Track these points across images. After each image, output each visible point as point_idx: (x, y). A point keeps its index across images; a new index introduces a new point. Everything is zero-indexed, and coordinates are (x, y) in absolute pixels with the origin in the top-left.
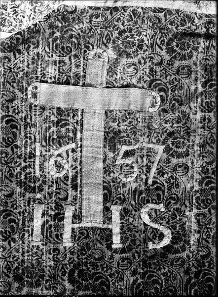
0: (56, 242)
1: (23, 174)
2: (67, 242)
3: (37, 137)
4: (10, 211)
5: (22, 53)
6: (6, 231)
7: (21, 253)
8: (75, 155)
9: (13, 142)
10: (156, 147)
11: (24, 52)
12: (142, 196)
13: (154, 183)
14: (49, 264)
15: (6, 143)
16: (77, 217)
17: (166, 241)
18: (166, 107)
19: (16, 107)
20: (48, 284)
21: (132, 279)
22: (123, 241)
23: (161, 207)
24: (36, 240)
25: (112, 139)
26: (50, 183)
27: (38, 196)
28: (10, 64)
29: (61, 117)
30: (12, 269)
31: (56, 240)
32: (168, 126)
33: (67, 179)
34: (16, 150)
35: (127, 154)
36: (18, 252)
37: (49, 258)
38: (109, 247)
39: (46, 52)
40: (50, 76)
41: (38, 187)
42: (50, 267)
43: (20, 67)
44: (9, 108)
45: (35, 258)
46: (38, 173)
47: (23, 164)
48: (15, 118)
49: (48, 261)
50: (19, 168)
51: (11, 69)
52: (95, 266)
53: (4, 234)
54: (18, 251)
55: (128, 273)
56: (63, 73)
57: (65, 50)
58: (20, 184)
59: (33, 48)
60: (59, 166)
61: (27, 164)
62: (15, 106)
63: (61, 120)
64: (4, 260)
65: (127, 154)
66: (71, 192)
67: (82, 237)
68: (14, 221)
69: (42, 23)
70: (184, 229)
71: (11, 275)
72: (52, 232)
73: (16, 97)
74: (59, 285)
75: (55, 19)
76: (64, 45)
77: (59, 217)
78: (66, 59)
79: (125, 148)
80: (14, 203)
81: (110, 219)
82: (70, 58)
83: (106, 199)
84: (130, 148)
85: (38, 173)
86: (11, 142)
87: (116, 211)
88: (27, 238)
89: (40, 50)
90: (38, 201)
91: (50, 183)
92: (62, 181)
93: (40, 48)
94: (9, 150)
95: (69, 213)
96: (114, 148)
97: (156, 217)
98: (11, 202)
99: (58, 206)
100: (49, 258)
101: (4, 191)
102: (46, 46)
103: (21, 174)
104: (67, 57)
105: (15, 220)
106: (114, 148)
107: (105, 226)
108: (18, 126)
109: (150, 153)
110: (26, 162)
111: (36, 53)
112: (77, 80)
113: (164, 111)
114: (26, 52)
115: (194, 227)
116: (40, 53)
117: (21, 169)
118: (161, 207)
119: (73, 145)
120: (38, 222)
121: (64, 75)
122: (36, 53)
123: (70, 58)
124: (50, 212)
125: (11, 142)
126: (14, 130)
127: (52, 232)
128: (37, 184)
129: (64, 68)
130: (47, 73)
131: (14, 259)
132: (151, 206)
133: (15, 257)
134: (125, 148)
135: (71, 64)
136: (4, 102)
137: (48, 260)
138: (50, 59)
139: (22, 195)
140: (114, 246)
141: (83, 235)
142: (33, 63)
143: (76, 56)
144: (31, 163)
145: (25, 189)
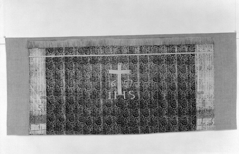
2: (115, 98)
10: (131, 80)
12: (129, 90)
13: (131, 87)
16: (117, 94)
17: (134, 97)
18: (133, 73)
21: (128, 105)
22: (126, 97)
23: (133, 91)
24: (110, 98)
25: (123, 79)
27: (110, 90)
32: (172, 120)
35: (126, 82)
38: (123, 99)
46: (109, 86)
49: (112, 102)
52: (121, 103)
55: (127, 104)
58: (144, 98)
60: (113, 84)
65: (126, 82)
66: (116, 89)
68: (68, 110)
70: (137, 95)
72: (113, 97)
77: (114, 94)
78: (151, 92)
79: (125, 81)
81: (123, 94)
83: (122, 90)
84: (126, 81)
85: (109, 86)
87: (124, 92)
89: (109, 64)
95: (115, 92)
96: (123, 81)
97: (132, 93)
99: (113, 92)
106: (123, 81)
107: (122, 95)
109: (130, 81)
112: (117, 69)
113: (132, 74)
115: (139, 95)
118: (133, 91)
119: (115, 80)
120: (110, 95)
127: (113, 97)
132: (131, 91)
134: (125, 81)
140: (124, 98)
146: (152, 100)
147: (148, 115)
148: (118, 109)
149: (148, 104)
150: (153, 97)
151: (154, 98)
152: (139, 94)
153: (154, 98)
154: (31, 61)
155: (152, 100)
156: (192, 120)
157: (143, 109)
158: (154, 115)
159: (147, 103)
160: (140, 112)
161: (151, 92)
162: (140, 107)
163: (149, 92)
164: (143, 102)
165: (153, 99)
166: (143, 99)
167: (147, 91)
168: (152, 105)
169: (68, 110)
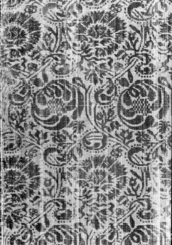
0: (59, 229)
1: (114, 185)
3: (93, 100)
4: (132, 128)
5: (121, 226)
6: (136, 97)
7: (114, 62)
8: (35, 220)
9: (132, 235)
11: (119, 227)
14: (70, 51)
15: (142, 234)
19: (127, 141)
20: (73, 164)
26: (72, 173)
28: (139, 209)
29: (58, 132)
30: (127, 185)
31: (60, 232)
33: (48, 182)
34: (126, 222)
36: (120, 210)
37: (71, 205)
39: (84, 86)
40: (78, 194)
41: (91, 166)
42: (69, 191)
43: (123, 58)
44: (137, 138)
45: (94, 201)
47: (114, 201)
48: (128, 126)
50: (121, 48)
51: (138, 200)
53: (139, 91)
54: (120, 212)
56: (57, 200)
57: (54, 91)
58: (120, 170)
59: (103, 90)
61: (108, 202)
62: (129, 142)
63: (58, 127)
64: (141, 197)
67: (20, 238)
68: (127, 113)
69: (94, 130)
71: (129, 175)
73: (127, 156)
74: (55, 19)
75: (75, 136)
76: (56, 97)
78: (53, 221)
80: (127, 141)
82: (47, 222)
86: (135, 235)
88: (104, 88)
89: (94, 87)
90: (91, 145)
91: (72, 173)
92: (54, 178)
93: (93, 91)
94: (138, 223)
98: (131, 141)
100: (71, 205)
101: (142, 158)
102: (85, 240)
103: (118, 186)
104: (50, 80)
105: (124, 114)
108: (122, 114)
110: (111, 204)
111: (99, 82)
114: (115, 227)
116: (93, 84)
117: (117, 47)
121: (56, 198)
122: (101, 227)
123: (47, 222)
124: (70, 130)
125: (135, 235)
126: (126, 107)
128: (93, 170)
129: (56, 207)
130: (81, 198)
131: (124, 54)
133: (125, 203)
135: (45, 215)
136: (145, 147)
137: (72, 202)
138: (78, 221)
139: (117, 152)
141: (19, 240)
142: (104, 212)
143: (37, 82)
144: (103, 202)
145: (110, 161)
146: (48, 151)
147: (81, 30)
148: (112, 142)
149: (82, 117)
150: (43, 176)
151: (37, 169)
152: (157, 208)
153: (34, 170)
154: (167, 69)
155: (48, 151)
156: (36, 55)
157: (123, 82)
158: (34, 25)
159: (90, 126)
160: (154, 52)
161: (53, 221)
162: (151, 97)
163: (70, 223)
164: (126, 137)
165: (39, 161)
166: (122, 160)
167: (90, 228)
168: (46, 113)
169: (127, 113)
